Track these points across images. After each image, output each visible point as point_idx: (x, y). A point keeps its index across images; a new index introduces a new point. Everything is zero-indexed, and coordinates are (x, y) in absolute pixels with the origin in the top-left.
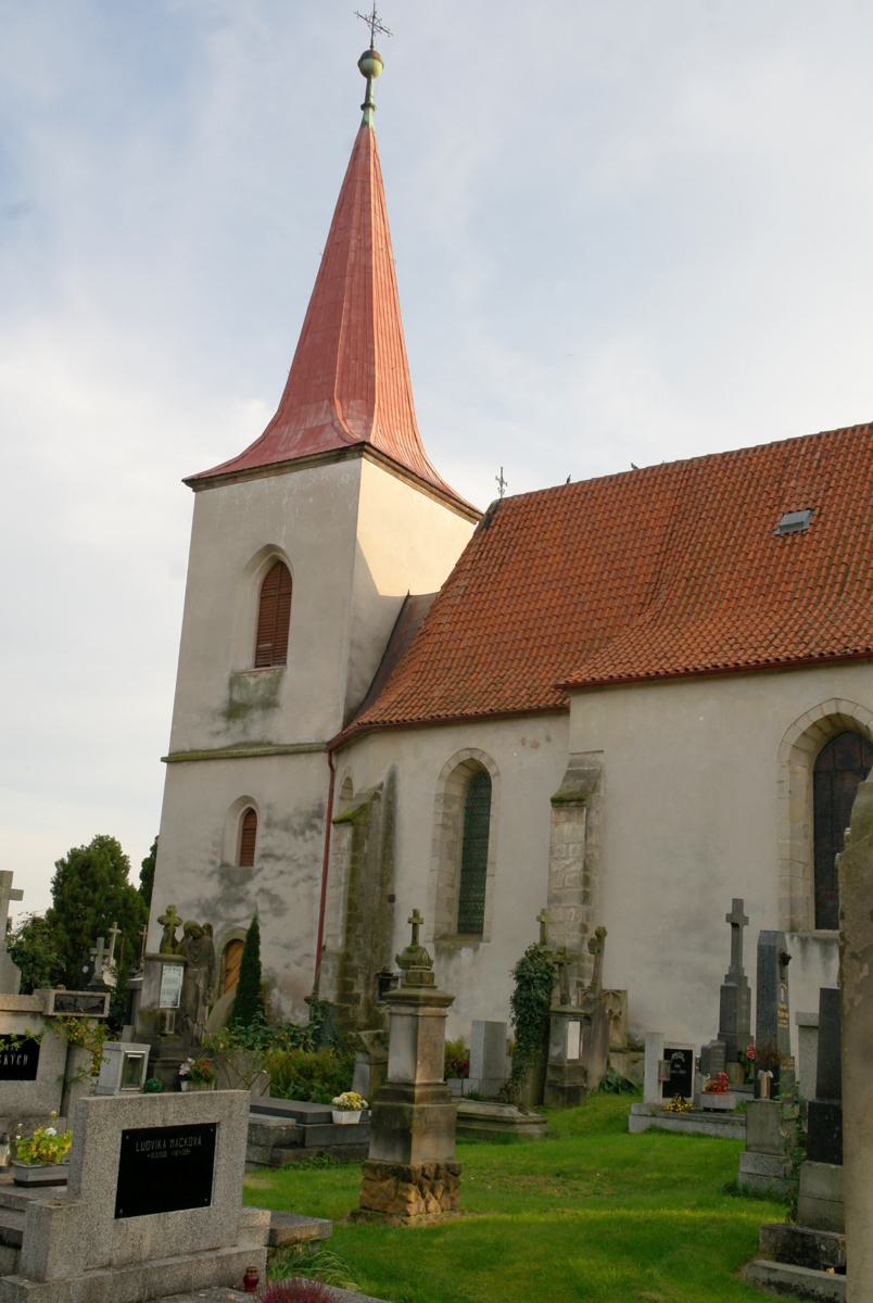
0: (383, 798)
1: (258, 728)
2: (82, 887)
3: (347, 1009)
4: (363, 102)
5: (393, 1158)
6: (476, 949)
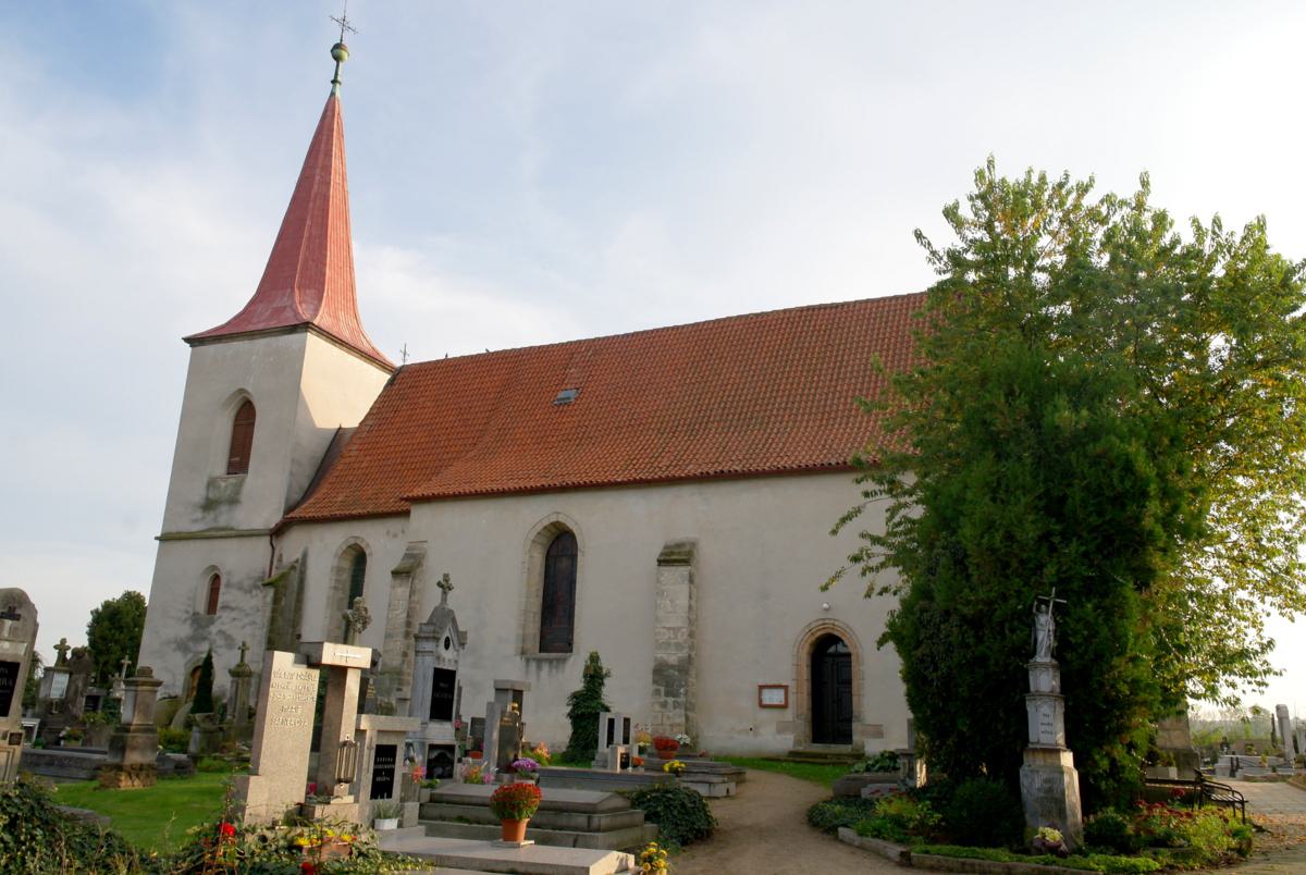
1: (225, 517)
2: (110, 630)
4: (333, 78)
5: (117, 760)
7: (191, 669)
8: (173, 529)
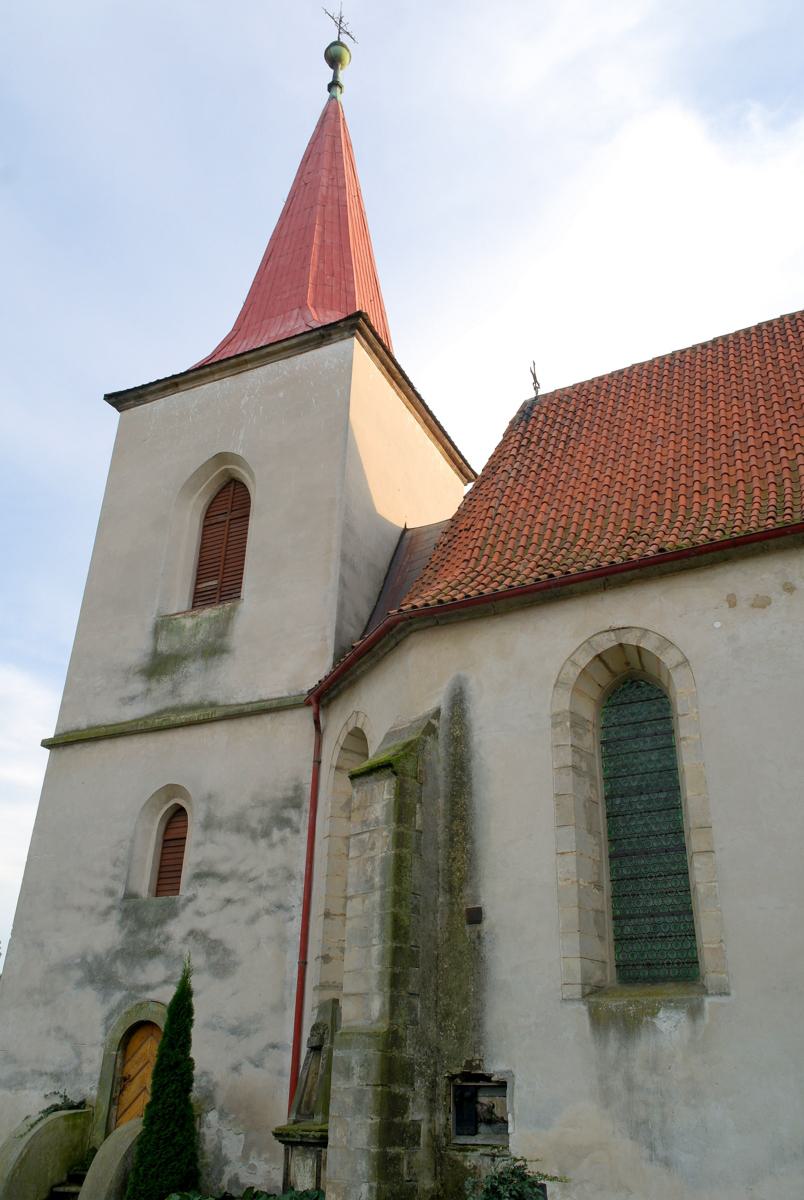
0: (442, 733)
1: (195, 686)
3: (397, 1158)
6: (695, 1012)
7: (120, 1035)
8: (82, 722)
